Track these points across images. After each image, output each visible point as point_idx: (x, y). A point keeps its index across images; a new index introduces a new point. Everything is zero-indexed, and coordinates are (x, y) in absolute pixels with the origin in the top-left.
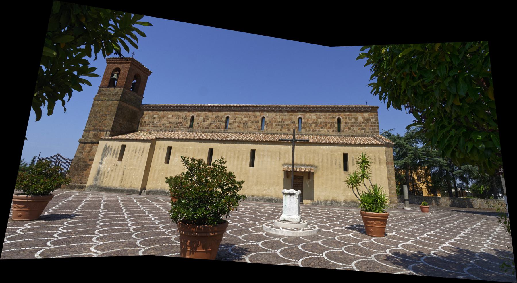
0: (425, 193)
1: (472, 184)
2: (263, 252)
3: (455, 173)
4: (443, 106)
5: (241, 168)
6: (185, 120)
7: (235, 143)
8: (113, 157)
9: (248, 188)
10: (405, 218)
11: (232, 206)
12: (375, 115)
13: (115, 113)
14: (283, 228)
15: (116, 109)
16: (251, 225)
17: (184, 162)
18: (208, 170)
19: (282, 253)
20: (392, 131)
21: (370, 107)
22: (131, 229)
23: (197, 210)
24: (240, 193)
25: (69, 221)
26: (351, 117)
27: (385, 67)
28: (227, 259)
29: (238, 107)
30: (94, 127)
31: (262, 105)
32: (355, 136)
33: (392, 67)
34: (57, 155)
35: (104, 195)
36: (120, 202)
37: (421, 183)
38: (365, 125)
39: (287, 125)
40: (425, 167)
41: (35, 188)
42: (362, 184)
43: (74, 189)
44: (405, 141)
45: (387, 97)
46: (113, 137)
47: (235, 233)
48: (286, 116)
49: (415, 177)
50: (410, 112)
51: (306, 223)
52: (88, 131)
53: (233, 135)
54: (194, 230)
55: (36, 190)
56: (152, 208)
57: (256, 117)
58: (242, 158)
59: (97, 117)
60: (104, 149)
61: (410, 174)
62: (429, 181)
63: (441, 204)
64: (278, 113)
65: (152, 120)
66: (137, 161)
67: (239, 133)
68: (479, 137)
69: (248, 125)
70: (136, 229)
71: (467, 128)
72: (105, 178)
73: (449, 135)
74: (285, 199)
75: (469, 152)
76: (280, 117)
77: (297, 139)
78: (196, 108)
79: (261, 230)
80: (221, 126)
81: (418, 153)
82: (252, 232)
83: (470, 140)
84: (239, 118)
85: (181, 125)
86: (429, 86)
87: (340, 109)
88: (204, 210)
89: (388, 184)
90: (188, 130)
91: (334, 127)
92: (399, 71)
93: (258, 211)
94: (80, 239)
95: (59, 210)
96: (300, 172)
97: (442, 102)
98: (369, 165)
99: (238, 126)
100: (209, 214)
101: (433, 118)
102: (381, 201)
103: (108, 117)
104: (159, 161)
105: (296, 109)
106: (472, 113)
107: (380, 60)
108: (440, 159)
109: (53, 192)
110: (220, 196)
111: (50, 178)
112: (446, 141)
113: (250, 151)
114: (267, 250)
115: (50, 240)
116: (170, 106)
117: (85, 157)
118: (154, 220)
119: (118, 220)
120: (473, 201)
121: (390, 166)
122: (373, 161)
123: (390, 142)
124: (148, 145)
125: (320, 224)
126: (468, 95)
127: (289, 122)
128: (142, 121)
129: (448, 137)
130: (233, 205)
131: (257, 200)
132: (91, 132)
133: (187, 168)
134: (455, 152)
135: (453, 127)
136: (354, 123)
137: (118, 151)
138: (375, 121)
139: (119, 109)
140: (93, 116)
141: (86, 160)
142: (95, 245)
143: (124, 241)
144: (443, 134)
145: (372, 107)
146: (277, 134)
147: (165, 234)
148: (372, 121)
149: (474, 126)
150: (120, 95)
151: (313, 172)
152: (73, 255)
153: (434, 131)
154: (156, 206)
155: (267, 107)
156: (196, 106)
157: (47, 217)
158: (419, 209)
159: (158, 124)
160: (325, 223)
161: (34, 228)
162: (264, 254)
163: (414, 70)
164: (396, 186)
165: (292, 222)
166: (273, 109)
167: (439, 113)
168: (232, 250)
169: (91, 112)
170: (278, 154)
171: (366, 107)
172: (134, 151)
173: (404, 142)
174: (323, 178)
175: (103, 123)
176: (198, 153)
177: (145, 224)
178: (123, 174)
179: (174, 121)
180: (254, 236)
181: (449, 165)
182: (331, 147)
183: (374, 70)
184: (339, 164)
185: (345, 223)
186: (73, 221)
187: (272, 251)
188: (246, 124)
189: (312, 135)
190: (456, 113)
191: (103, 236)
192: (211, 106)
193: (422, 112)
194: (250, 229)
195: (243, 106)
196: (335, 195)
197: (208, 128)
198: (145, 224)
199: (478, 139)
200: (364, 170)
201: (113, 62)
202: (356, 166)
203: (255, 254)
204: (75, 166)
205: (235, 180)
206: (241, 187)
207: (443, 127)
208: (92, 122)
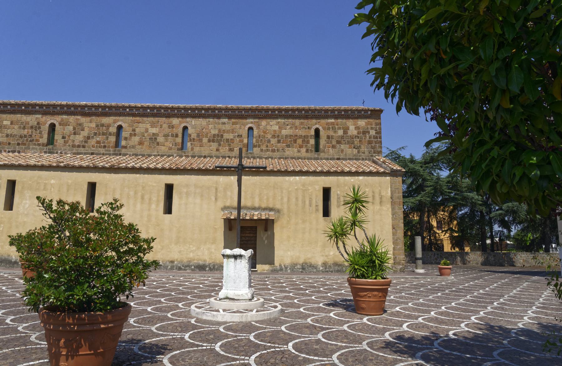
0: (447, 247)
1: (516, 231)
2: (192, 349)
3: (493, 216)
4: (485, 108)
5: (149, 216)
6: (38, 131)
7: (136, 174)
9: (162, 249)
10: (415, 285)
11: (136, 280)
12: (376, 123)
14: (224, 310)
16: (170, 309)
17: (43, 207)
18: (91, 222)
19: (223, 348)
20: (403, 150)
21: (369, 110)
23: (74, 288)
24: (149, 257)
26: (337, 127)
27: (396, 41)
28: (132, 363)
29: (139, 107)
31: (182, 106)
32: (343, 159)
33: (408, 40)
37: (443, 231)
38: (360, 141)
39: (227, 140)
40: (449, 207)
42: (351, 237)
44: (421, 167)
45: (397, 93)
48: (227, 125)
49: (434, 223)
50: (432, 119)
51: (262, 300)
57: (172, 127)
58: (150, 199)
61: (426, 219)
62: (454, 229)
63: (469, 262)
64: (211, 120)
67: (143, 156)
68: (532, 160)
69: (158, 140)
71: (517, 145)
73: (490, 155)
75: (517, 183)
77: (246, 165)
78: (58, 108)
79: (188, 315)
80: (109, 143)
81: (440, 185)
83: (520, 164)
85: (31, 141)
86: (464, 75)
87: (320, 114)
88: (87, 287)
89: (392, 235)
91: (309, 145)
92: (420, 48)
93: (181, 285)
96: (252, 220)
97: (483, 102)
98: (364, 206)
99: (141, 143)
100: (95, 294)
101: (467, 128)
102: (381, 261)
105: (243, 112)
106: (526, 120)
107: (388, 27)
108: (473, 195)
110: (113, 263)
112: (483, 166)
113: (164, 186)
114: (198, 346)
120: (515, 256)
121: (397, 208)
122: (370, 199)
123: (399, 168)
125: (285, 301)
126: (524, 92)
127: (230, 136)
129: (487, 159)
130: (137, 278)
131: (180, 269)
133: (51, 218)
134: (497, 182)
135: (496, 144)
136: (342, 137)
138: (376, 133)
144: (481, 155)
145: (371, 111)
146: (211, 157)
148: (371, 134)
149: (527, 142)
151: (273, 220)
153: (467, 150)
155: (191, 109)
156: (58, 105)
158: (436, 272)
160: (292, 298)
162: (194, 351)
163: (444, 46)
164: (404, 238)
165: (239, 300)
166: (203, 112)
167: (477, 121)
168: (140, 349)
170: (214, 191)
171: (363, 110)
173: (420, 168)
174: (290, 228)
176: (68, 191)
179: (15, 133)
180: (177, 324)
181: (485, 204)
182: (303, 177)
183: (378, 45)
184: (317, 206)
185: (324, 298)
187: (206, 346)
188: (153, 138)
189: (272, 158)
190: (503, 120)
192: (86, 106)
193: (452, 118)
194: (169, 315)
195: (148, 107)
196: (309, 256)
197: (84, 147)
199: (531, 162)
200: (355, 214)
202: (343, 207)
203: (178, 352)
205: (139, 236)
206: (150, 248)
207: (482, 143)
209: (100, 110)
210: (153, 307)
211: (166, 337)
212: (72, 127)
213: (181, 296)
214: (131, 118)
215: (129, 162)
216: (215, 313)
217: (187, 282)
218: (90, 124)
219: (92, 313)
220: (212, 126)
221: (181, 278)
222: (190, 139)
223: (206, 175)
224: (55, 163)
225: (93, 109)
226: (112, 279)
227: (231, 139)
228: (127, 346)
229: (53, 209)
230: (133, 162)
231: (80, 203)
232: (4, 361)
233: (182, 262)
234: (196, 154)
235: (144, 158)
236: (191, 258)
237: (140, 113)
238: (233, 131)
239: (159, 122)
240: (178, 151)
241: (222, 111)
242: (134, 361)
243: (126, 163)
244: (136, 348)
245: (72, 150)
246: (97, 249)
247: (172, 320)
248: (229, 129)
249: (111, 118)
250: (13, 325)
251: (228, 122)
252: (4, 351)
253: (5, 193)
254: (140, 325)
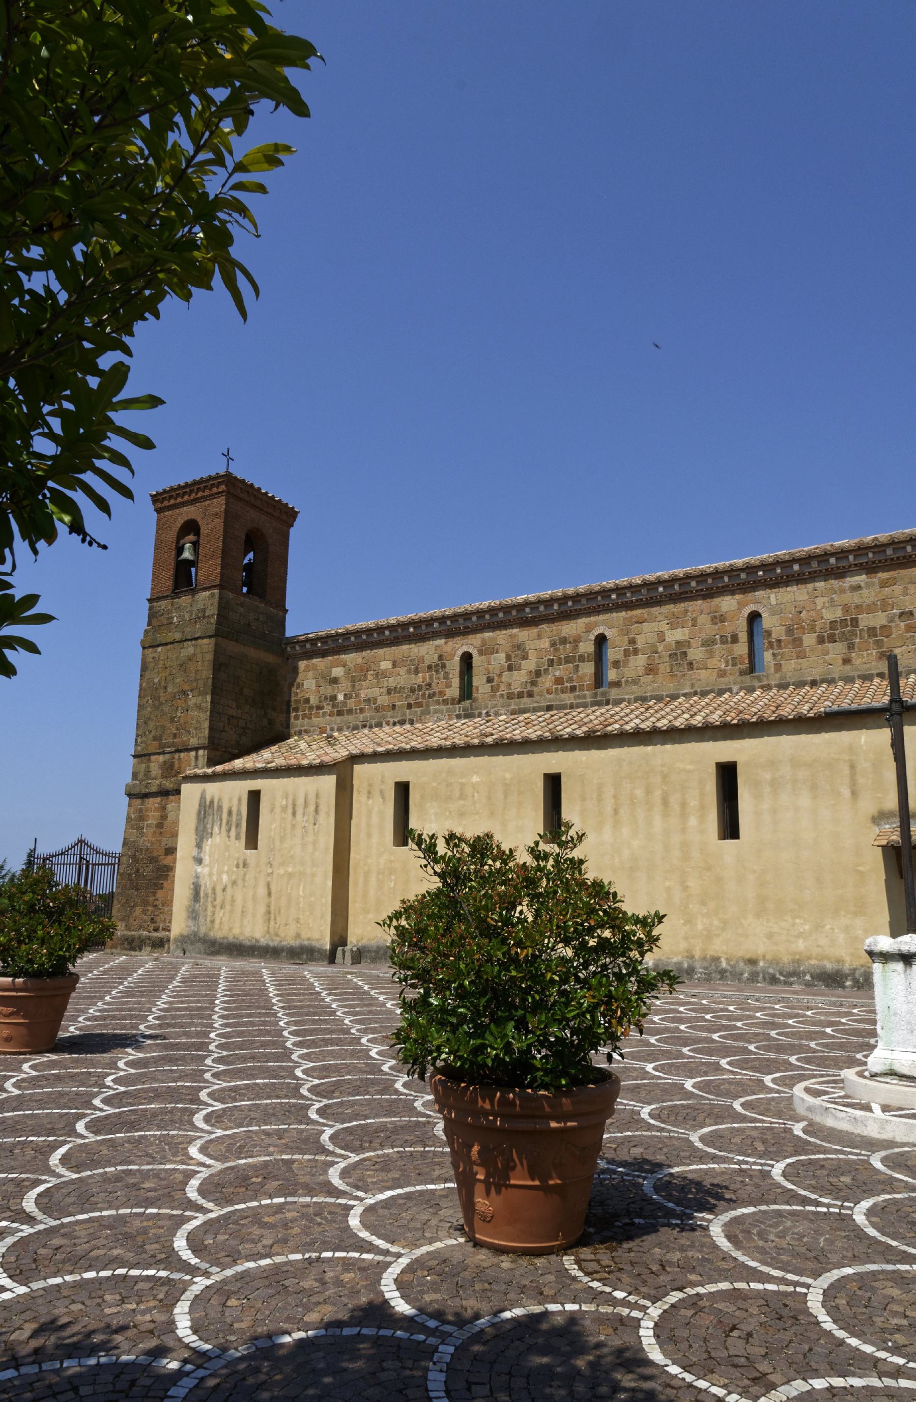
2: (788, 1207)
5: (685, 846)
6: (442, 675)
7: (646, 745)
8: (229, 837)
9: (723, 929)
13: (210, 681)
14: (885, 1108)
15: (211, 667)
16: (741, 1089)
17: (420, 849)
19: (874, 1219)
25: (131, 1058)
28: (636, 1221)
30: (161, 740)
31: (739, 562)
34: (79, 841)
35: (225, 967)
36: (272, 990)
39: (872, 631)
41: (28, 954)
43: (141, 950)
46: (219, 768)
47: (672, 1118)
48: (865, 592)
52: (145, 755)
53: (632, 711)
54: (487, 1106)
55: (30, 961)
56: (370, 1012)
57: (719, 618)
58: (683, 805)
59: (161, 704)
60: (199, 813)
64: (820, 585)
65: (328, 690)
66: (304, 845)
67: (659, 699)
69: (690, 657)
70: (318, 1089)
72: (218, 908)
74: (884, 978)
76: (832, 600)
78: (474, 618)
79: (785, 1108)
80: (581, 678)
82: (744, 1119)
84: (646, 634)
85: (430, 696)
90: (458, 709)
93: (774, 1026)
94: (160, 1117)
95: (105, 1018)
99: (651, 670)
103: (192, 700)
104: (375, 839)
109: (74, 966)
111: (60, 922)
113: (713, 770)
114: (805, 1201)
115: (84, 1116)
116: (380, 629)
117: (152, 843)
118: (377, 1057)
119: (265, 1055)
124: (328, 782)
127: (879, 619)
128: (298, 698)
131: (773, 980)
132: (153, 758)
137: (239, 813)
139: (218, 666)
140: (150, 701)
141: (155, 854)
142: (200, 1137)
143: (285, 1130)
146: (831, 681)
147: (413, 1111)
150: (212, 616)
152: (143, 1167)
154: (384, 1005)
155: (763, 566)
156: (472, 613)
157: (75, 1044)
159: (351, 703)
161: (43, 1076)
162: (793, 1213)
166: (796, 567)
168: (657, 1189)
169: (141, 689)
170: (846, 771)
172: (290, 811)
175: (182, 721)
176: (506, 797)
177: (350, 1069)
178: (269, 894)
179: (402, 684)
180: (754, 1134)
186: (141, 1055)
187: (828, 1206)
188: (679, 653)
191: (224, 1110)
192: (527, 603)
194: (737, 1105)
195: (659, 582)
197: (530, 695)
198: (350, 1069)
201: (172, 501)
203: (750, 1210)
204: (130, 875)
206: (654, 940)
208: (151, 725)
209: (556, 607)
210: (699, 1079)
211: (722, 1166)
212: (503, 655)
213: (772, 1055)
214: (624, 613)
215: (627, 719)
216: (859, 1113)
217: (791, 1016)
218: (537, 642)
219: (529, 1091)
220: (825, 599)
221: (777, 1007)
222: (770, 643)
223: (818, 731)
224: (477, 737)
225: (542, 608)
226: (563, 1013)
227: (883, 627)
228: (627, 1175)
229: (439, 855)
230: (637, 717)
231: (492, 837)
232: (383, 1174)
233: (778, 963)
234: (788, 680)
235: (662, 705)
236: (800, 954)
237: (642, 600)
238: (885, 605)
239: (687, 611)
240: (743, 678)
241: (847, 557)
242: (640, 1217)
243: (622, 722)
244: (647, 1184)
245: (509, 705)
246: (528, 944)
247: (744, 1119)
248: (871, 600)
249: (579, 621)
250: (407, 1095)
251: (867, 583)
252: (386, 1151)
253: (392, 811)
254: (663, 1125)
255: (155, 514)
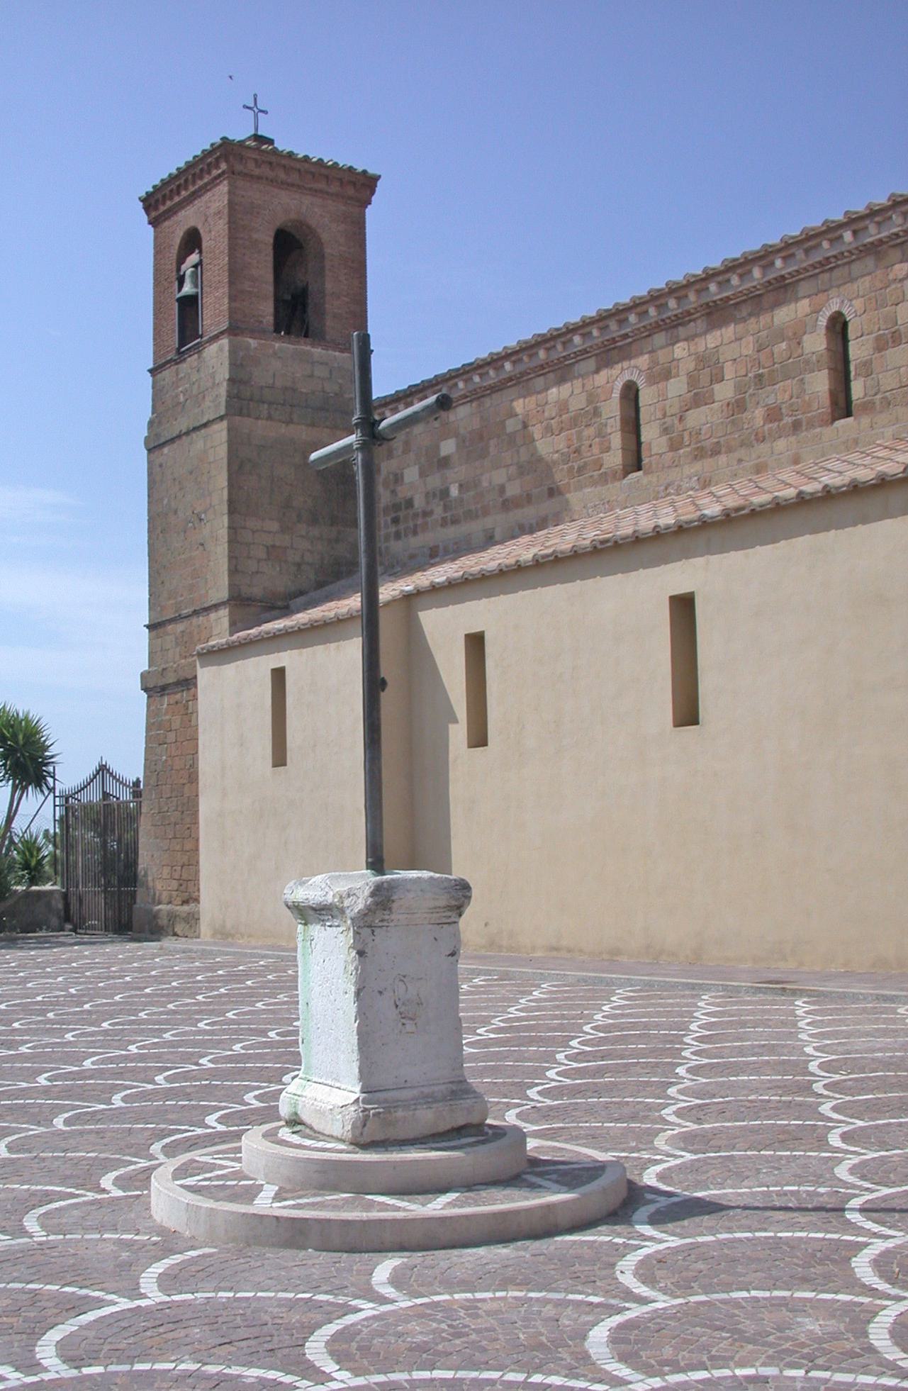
22: (847, 1164)
255: (151, 229)
